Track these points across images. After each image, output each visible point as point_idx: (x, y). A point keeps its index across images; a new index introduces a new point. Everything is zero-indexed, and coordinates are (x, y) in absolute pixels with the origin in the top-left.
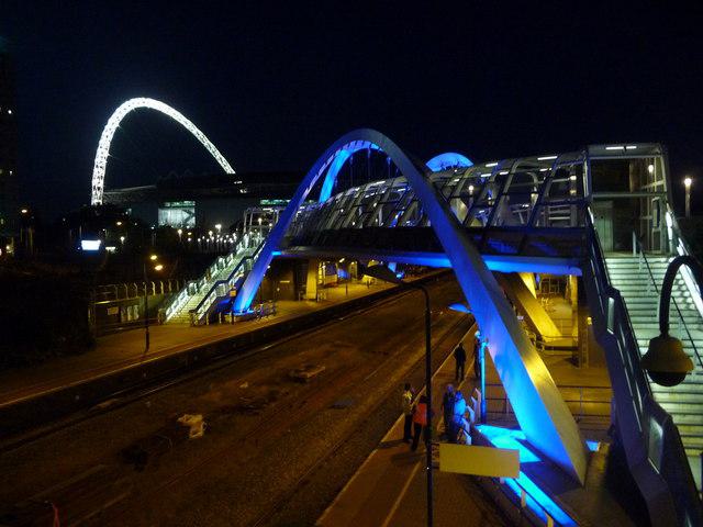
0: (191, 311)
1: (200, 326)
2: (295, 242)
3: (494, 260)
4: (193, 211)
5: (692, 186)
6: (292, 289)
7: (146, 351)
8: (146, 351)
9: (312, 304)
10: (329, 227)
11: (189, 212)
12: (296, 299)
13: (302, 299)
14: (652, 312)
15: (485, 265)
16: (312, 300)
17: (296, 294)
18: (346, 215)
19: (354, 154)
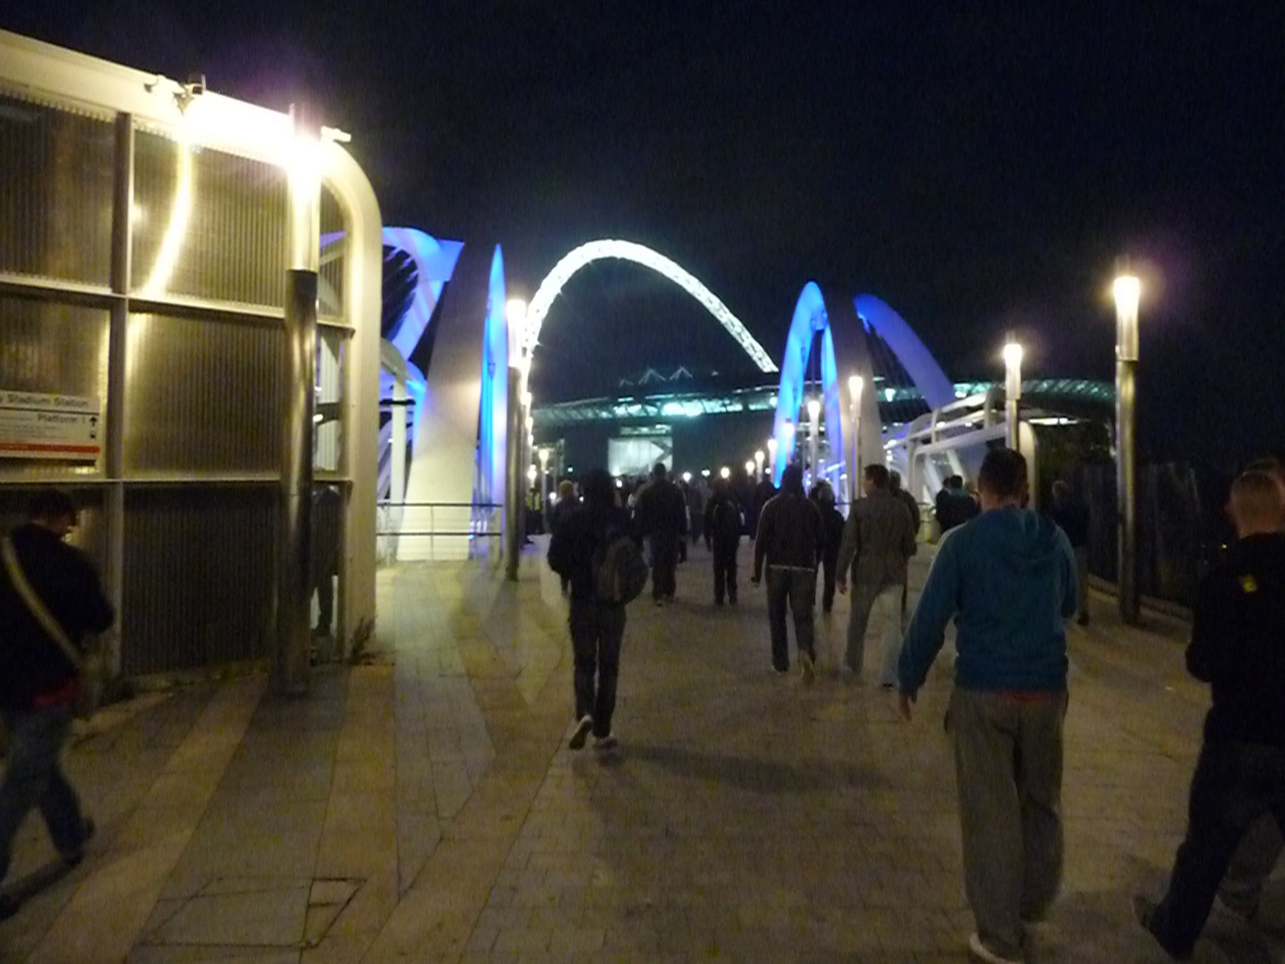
4: (669, 443)
11: (663, 447)
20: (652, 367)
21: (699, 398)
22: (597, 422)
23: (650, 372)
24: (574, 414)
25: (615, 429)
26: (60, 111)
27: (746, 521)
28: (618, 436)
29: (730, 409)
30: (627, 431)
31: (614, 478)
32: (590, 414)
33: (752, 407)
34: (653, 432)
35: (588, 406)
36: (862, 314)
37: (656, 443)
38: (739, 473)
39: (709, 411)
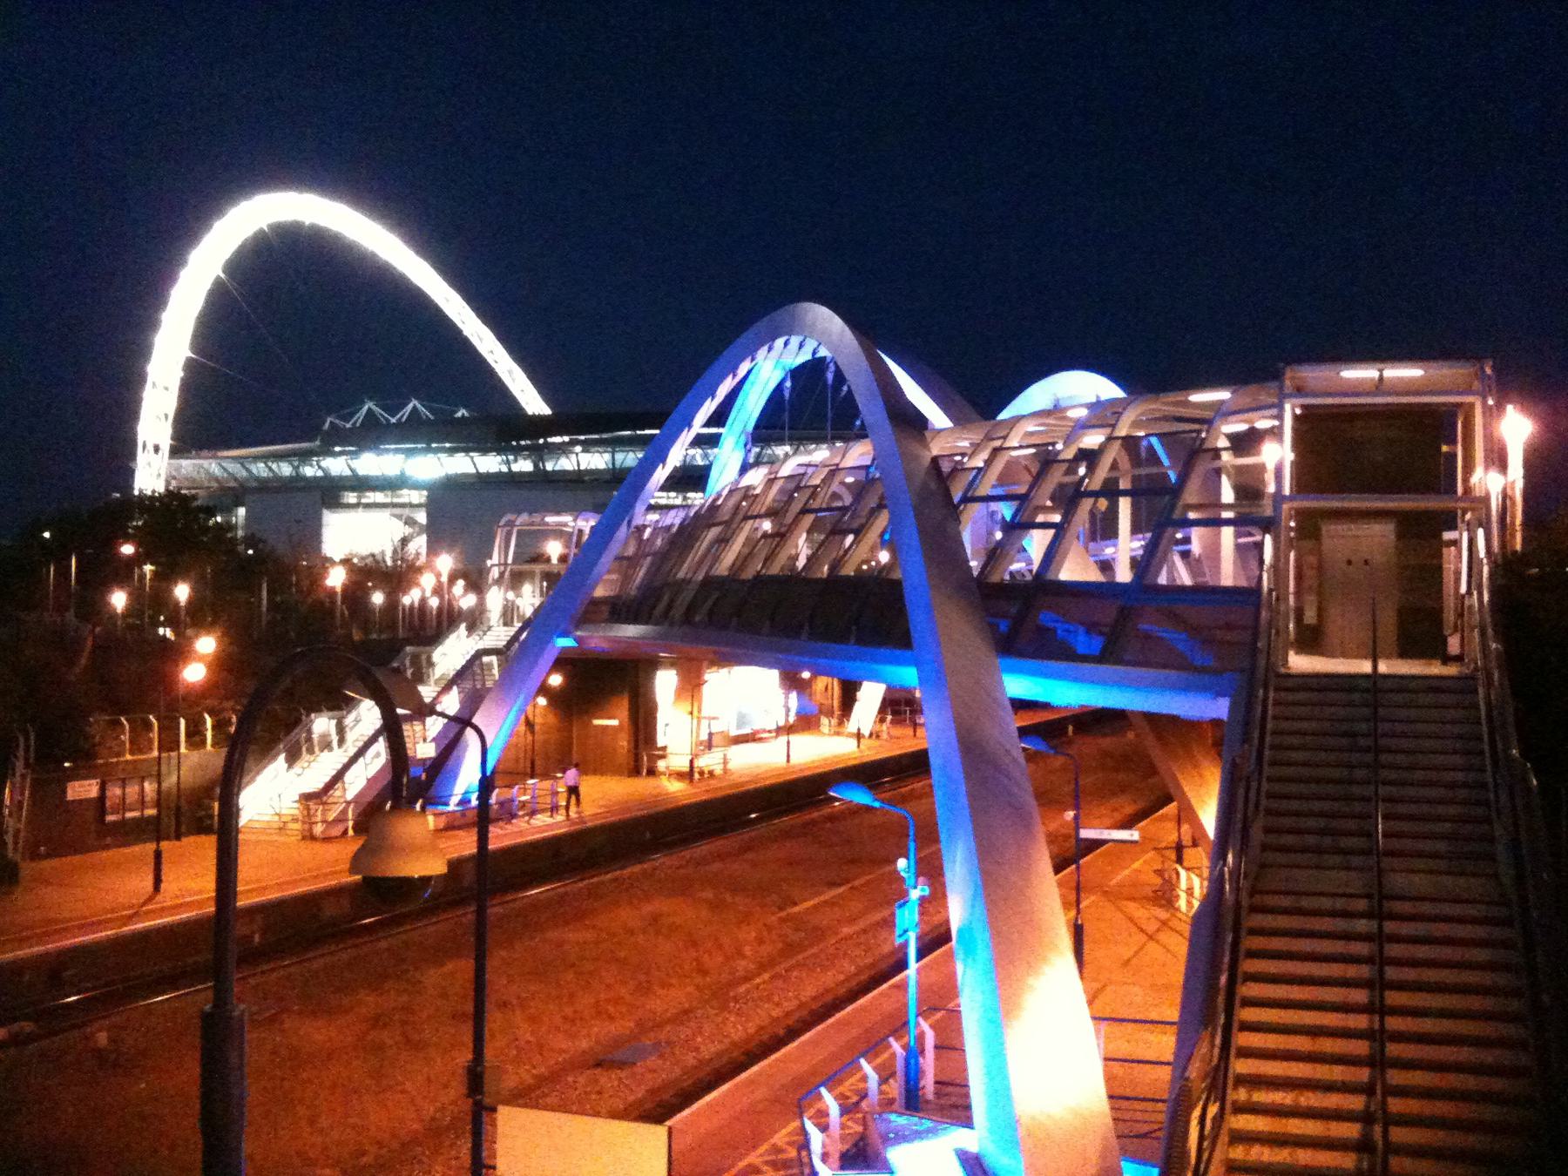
0: (307, 798)
1: (327, 839)
2: (620, 610)
3: (1020, 671)
4: (421, 517)
5: (190, 602)
6: (624, 743)
7: (150, 900)
8: (150, 900)
9: (675, 787)
10: (724, 565)
11: (410, 522)
12: (635, 771)
13: (652, 772)
14: (1274, 804)
15: (1001, 683)
16: (680, 776)
17: (637, 758)
18: (781, 536)
19: (796, 373)
20: (371, 399)
21: (467, 450)
22: (297, 485)
23: (414, 403)
24: (234, 468)
25: (330, 493)
26: (1145, 551)
27: (346, 695)
28: (335, 504)
29: (516, 468)
30: (351, 498)
31: (328, 562)
32: (286, 469)
33: (549, 466)
34: (396, 500)
35: (256, 458)
36: (1536, 574)
37: (399, 517)
38: (392, 604)
39: (482, 470)
